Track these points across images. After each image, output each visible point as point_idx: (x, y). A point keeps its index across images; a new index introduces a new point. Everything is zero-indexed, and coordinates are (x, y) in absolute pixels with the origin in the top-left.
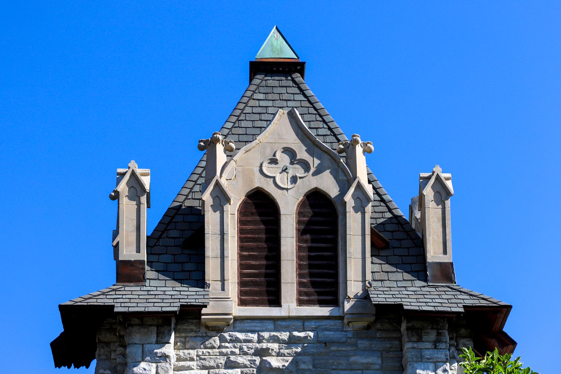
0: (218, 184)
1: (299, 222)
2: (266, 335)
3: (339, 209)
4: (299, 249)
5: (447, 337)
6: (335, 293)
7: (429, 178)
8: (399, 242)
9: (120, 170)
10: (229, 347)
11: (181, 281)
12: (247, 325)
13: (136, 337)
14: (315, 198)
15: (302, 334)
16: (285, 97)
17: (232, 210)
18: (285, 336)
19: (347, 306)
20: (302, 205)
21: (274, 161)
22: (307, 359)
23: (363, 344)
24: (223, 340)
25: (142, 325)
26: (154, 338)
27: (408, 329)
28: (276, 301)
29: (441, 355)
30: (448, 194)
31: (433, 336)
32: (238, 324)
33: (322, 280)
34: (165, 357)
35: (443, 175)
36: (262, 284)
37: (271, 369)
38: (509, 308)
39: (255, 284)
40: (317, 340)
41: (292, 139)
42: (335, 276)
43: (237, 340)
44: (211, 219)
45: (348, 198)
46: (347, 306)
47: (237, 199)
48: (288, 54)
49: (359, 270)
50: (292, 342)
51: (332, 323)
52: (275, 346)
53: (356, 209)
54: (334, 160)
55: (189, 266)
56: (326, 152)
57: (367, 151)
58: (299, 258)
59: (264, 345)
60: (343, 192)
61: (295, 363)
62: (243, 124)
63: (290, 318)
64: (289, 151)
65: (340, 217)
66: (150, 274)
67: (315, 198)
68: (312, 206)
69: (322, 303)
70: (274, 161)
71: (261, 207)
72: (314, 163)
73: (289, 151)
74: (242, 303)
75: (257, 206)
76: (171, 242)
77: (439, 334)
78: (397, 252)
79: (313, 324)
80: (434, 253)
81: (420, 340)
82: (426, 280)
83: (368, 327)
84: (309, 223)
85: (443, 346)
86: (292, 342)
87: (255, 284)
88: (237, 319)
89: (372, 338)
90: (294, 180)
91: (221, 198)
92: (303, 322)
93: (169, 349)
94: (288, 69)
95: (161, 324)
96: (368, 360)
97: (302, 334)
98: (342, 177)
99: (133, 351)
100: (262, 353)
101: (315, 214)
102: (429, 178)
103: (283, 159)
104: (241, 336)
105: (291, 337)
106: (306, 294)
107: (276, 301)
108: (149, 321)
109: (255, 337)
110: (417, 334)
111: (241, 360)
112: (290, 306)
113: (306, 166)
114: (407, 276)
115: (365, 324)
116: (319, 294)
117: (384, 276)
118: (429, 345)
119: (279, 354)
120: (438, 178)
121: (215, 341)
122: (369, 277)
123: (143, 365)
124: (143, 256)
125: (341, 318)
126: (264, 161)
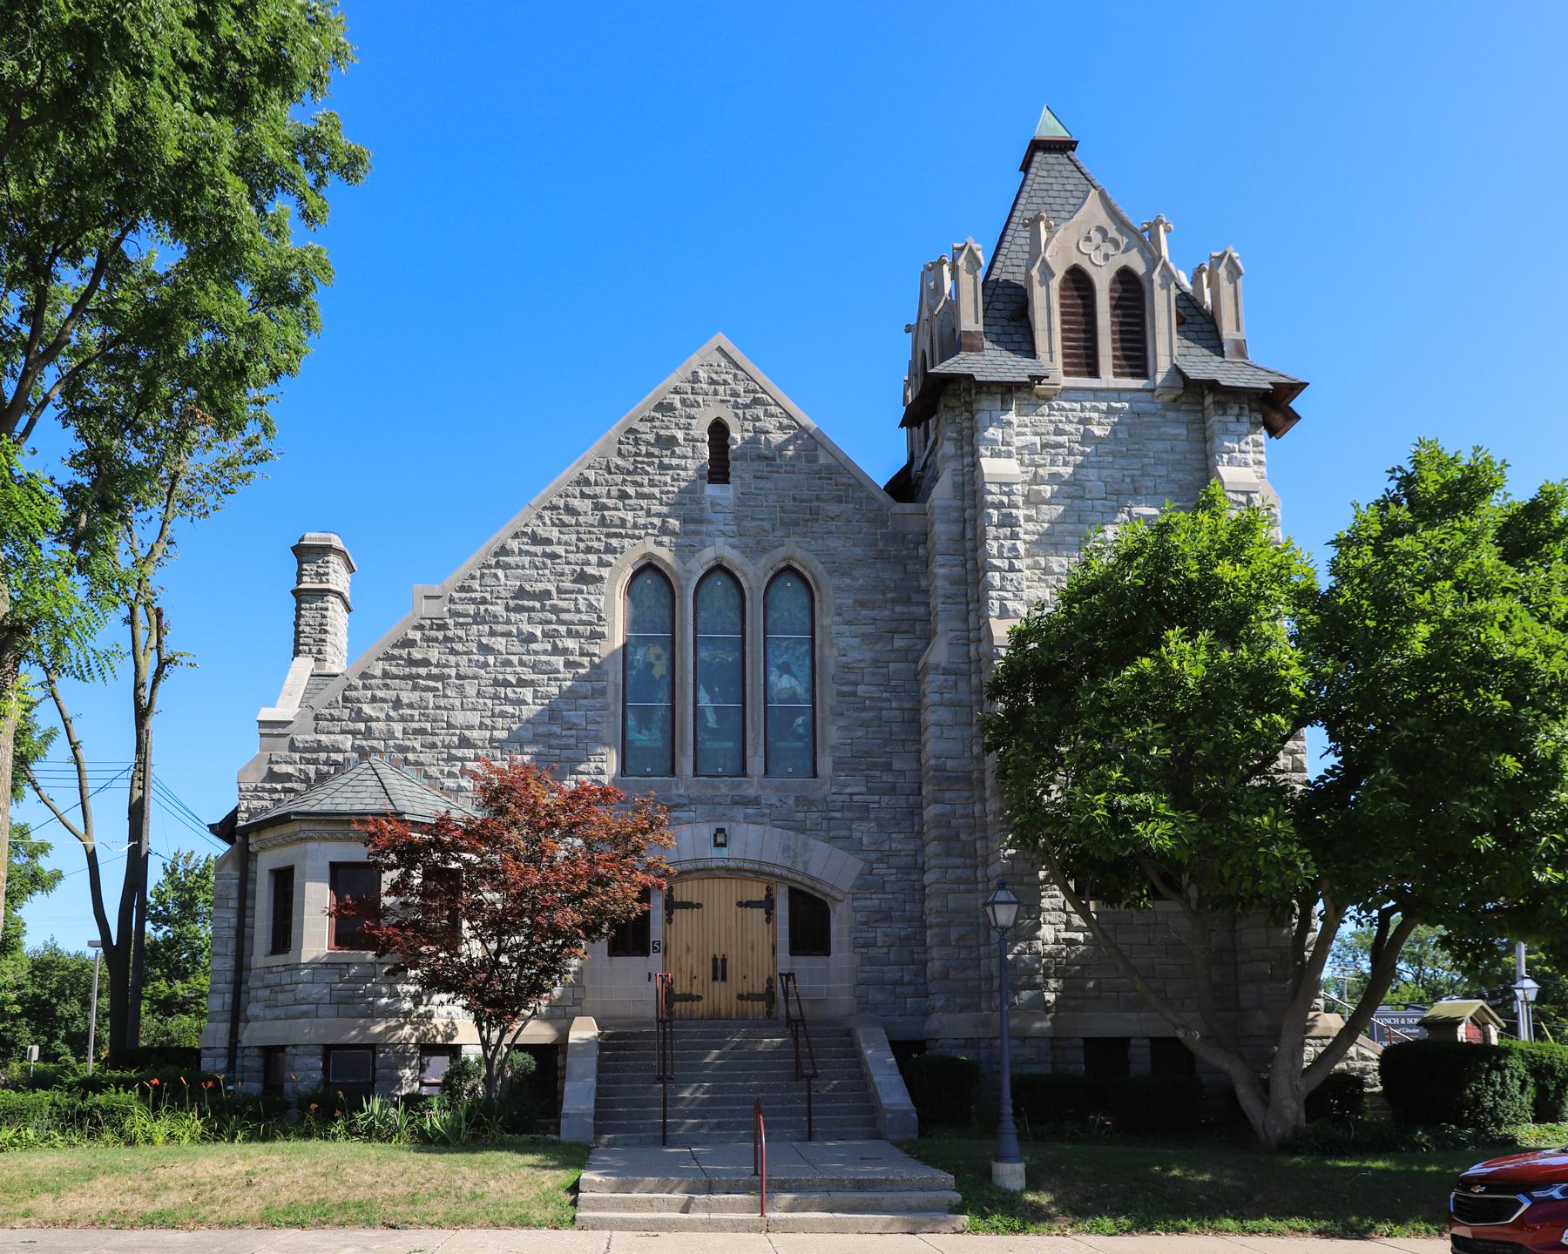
0: (1044, 260)
1: (1112, 298)
2: (1088, 405)
3: (1146, 286)
4: (1113, 323)
5: (1246, 412)
6: (1145, 367)
7: (962, 249)
8: (1199, 322)
9: (957, 245)
10: (1057, 416)
11: (1013, 351)
12: (1072, 395)
13: (986, 404)
14: (1125, 277)
15: (1119, 405)
16: (1065, 174)
17: (1055, 284)
18: (1103, 406)
19: (1159, 378)
20: (1114, 281)
21: (1088, 239)
22: (1123, 428)
23: (1172, 415)
24: (1051, 408)
25: (989, 393)
26: (999, 406)
27: (1214, 403)
28: (1094, 373)
29: (1245, 427)
30: (1240, 273)
31: (1236, 410)
32: (1064, 395)
33: (1135, 357)
34: (1009, 423)
35: (975, 246)
36: (1084, 359)
37: (1094, 437)
38: (1306, 384)
39: (1075, 356)
40: (1132, 411)
41: (1104, 220)
42: (1144, 349)
43: (1063, 409)
44: (1038, 294)
45: (1156, 276)
46: (1159, 378)
47: (1060, 274)
48: (1059, 133)
49: (1167, 347)
50: (1110, 412)
51: (1143, 394)
52: (1095, 415)
53: (1162, 287)
54: (1142, 239)
55: (1017, 338)
56: (1134, 231)
57: (1167, 231)
58: (1113, 332)
59: (1087, 414)
60: (1150, 271)
61: (1113, 431)
62: (1035, 200)
63: (1108, 390)
64: (1101, 230)
65: (1147, 295)
66: (987, 344)
67: (1125, 277)
68: (1122, 282)
69: (1133, 375)
70: (1088, 239)
71: (1078, 281)
72: (1123, 241)
73: (1101, 230)
74: (1066, 374)
75: (1074, 281)
76: (997, 314)
77: (1241, 409)
78: (1192, 327)
79: (1128, 396)
80: (1228, 331)
81: (1225, 414)
82: (1223, 356)
83: (1175, 400)
84: (1120, 298)
85: (1245, 419)
86: (1110, 412)
87: (1075, 356)
88: (1065, 389)
89: (1178, 410)
90: (1106, 257)
91: (1047, 272)
92: (1119, 393)
93: (1012, 416)
94: (1063, 147)
95: (1008, 391)
96: (1177, 430)
97: (1119, 405)
98: (1148, 255)
99: (982, 417)
100: (1084, 421)
101: (1124, 290)
102: (962, 249)
103: (1097, 237)
104: (1067, 405)
105: (1109, 407)
106: (1120, 366)
107: (1094, 373)
108: (995, 389)
109: (1077, 406)
110: (1222, 407)
111: (1068, 428)
112: (1108, 378)
113: (1116, 244)
114: (1206, 352)
115: (1172, 397)
116: (1131, 366)
117: (1185, 351)
118: (1233, 419)
119: (1099, 424)
120: (1230, 258)
121: (1045, 409)
122: (1175, 352)
123: (991, 430)
124: (980, 327)
125: (1152, 391)
126: (1075, 241)
